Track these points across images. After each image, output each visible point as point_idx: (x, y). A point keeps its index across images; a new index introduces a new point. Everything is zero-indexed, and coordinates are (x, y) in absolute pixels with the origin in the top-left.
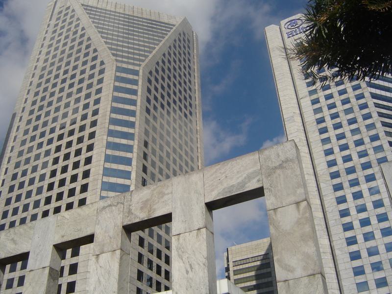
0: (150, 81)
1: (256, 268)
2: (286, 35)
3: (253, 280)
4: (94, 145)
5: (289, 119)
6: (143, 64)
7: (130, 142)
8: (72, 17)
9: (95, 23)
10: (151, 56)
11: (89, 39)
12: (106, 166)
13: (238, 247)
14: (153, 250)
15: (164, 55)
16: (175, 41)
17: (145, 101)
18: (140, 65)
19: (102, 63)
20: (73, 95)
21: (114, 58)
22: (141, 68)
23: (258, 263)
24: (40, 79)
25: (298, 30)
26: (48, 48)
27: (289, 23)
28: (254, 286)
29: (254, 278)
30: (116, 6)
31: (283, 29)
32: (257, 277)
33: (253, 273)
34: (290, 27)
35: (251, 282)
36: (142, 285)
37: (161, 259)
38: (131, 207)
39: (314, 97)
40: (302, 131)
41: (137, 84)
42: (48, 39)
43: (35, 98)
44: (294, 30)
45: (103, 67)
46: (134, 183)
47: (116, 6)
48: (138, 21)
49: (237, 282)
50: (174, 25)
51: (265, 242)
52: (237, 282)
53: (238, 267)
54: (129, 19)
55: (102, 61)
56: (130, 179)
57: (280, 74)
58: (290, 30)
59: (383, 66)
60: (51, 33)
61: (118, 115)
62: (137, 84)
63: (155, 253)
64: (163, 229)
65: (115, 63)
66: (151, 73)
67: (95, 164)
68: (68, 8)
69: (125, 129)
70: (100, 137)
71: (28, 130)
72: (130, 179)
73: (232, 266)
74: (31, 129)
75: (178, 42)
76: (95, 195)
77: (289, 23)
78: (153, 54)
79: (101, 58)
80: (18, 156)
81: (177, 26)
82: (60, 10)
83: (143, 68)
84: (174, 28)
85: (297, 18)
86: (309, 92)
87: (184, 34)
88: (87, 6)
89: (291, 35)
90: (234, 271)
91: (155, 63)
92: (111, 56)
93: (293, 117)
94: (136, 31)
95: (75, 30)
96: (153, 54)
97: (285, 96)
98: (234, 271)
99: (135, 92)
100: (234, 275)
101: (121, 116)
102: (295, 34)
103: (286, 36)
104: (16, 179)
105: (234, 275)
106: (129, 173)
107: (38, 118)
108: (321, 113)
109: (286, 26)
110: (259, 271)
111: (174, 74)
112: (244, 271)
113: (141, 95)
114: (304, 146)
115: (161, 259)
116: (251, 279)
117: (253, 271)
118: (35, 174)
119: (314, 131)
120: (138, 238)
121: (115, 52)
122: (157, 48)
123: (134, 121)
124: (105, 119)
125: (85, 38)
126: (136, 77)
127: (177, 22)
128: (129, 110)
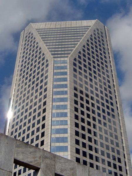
0: (75, 64)
6: (69, 56)
8: (32, 38)
11: (40, 48)
15: (84, 46)
16: (91, 36)
18: (67, 57)
21: (53, 56)
22: (68, 58)
37: (119, 166)
45: (47, 63)
47: (56, 25)
50: (90, 26)
56: (67, 125)
59: (10, 115)
61: (57, 89)
64: (93, 150)
65: (53, 59)
69: (62, 96)
71: (45, 92)
74: (38, 95)
76: (48, 138)
78: (76, 48)
84: (90, 28)
87: (98, 30)
88: (39, 29)
91: (77, 53)
92: (51, 55)
95: (33, 45)
104: (34, 126)
106: (67, 129)
107: (41, 87)
111: (92, 56)
113: (69, 74)
115: (119, 166)
121: (54, 53)
122: (79, 43)
123: (67, 90)
125: (39, 48)
127: (92, 24)
128: (63, 84)
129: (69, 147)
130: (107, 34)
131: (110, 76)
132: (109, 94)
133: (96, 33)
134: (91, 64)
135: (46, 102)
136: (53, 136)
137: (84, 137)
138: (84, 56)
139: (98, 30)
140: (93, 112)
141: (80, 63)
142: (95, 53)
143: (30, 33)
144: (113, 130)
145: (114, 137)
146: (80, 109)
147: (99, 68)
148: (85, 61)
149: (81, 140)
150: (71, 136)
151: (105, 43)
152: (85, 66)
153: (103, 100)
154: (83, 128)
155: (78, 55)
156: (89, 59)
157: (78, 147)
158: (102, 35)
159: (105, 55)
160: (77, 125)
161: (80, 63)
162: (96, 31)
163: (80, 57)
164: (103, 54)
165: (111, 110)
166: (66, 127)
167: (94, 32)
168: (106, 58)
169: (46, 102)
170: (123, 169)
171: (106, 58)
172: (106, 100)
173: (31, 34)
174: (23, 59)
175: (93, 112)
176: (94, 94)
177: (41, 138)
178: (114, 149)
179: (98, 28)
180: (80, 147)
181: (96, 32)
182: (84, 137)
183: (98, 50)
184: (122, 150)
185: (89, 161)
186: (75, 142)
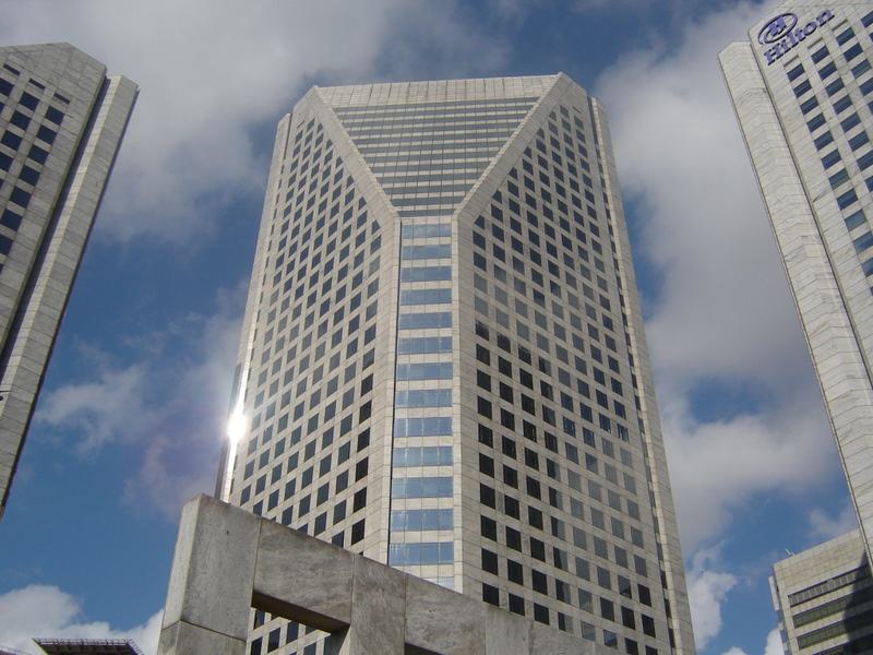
0: (479, 240)
1: (844, 605)
2: (765, 57)
3: (840, 634)
5: (793, 254)
6: (459, 207)
8: (319, 140)
9: (355, 133)
10: (477, 184)
13: (795, 558)
14: (630, 588)
18: (451, 212)
19: (376, 226)
20: (331, 306)
21: (398, 209)
22: (455, 217)
23: (848, 591)
25: (788, 40)
27: (767, 30)
28: (845, 646)
29: (842, 629)
30: (408, 92)
31: (757, 46)
32: (849, 625)
33: (838, 617)
34: (770, 38)
35: (837, 638)
38: (365, 555)
39: (843, 188)
40: (827, 277)
44: (780, 41)
45: (377, 234)
46: (460, 472)
48: (475, 110)
49: (804, 641)
51: (856, 540)
52: (804, 642)
53: (802, 606)
54: (435, 113)
55: (376, 221)
56: (450, 463)
57: (763, 153)
58: (771, 46)
63: (635, 594)
65: (398, 221)
67: (374, 445)
68: (311, 124)
70: (381, 386)
72: (450, 463)
73: (788, 606)
77: (767, 30)
78: (482, 179)
81: (543, 97)
83: (460, 215)
84: (536, 105)
85: (783, 13)
86: (830, 179)
87: (564, 111)
89: (775, 56)
90: (795, 617)
93: (802, 247)
94: (460, 137)
95: (325, 168)
96: (482, 179)
97: (779, 201)
98: (795, 617)
99: (445, 274)
100: (797, 626)
101: (420, 331)
102: (782, 51)
103: (764, 60)
105: (797, 626)
108: (864, 225)
109: (762, 39)
110: (852, 609)
112: (818, 614)
114: (836, 312)
116: (835, 630)
117: (838, 611)
118: (340, 472)
119: (853, 271)
122: (494, 161)
124: (388, 346)
125: (344, 180)
128: (436, 314)
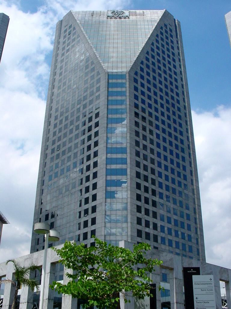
0: (136, 81)
4: (99, 141)
7: (124, 156)
12: (108, 167)
17: (133, 99)
24: (63, 50)
26: (64, 33)
36: (141, 240)
41: (126, 163)
42: (61, 43)
43: (63, 52)
60: (63, 33)
62: (126, 163)
66: (136, 73)
75: (160, 36)
79: (97, 69)
80: (52, 153)
82: (65, 29)
87: (166, 26)
106: (126, 170)
120: (136, 207)
126: (124, 166)
129: (128, 171)
130: (178, 31)
131: (175, 42)
132: (178, 120)
133: (163, 31)
134: (157, 79)
135: (98, 122)
136: (110, 90)
137: (146, 179)
138: (148, 67)
139: (166, 26)
140: (156, 110)
141: (142, 77)
142: (162, 61)
143: (70, 27)
144: (181, 168)
145: (183, 177)
146: (142, 142)
147: (164, 62)
148: (148, 74)
149: (143, 184)
150: (131, 179)
151: (175, 45)
152: (149, 82)
153: (171, 129)
154: (145, 168)
155: (139, 67)
156: (154, 71)
157: (139, 192)
158: (172, 34)
159: (174, 63)
160: (138, 164)
161: (142, 77)
162: (164, 28)
163: (142, 70)
164: (172, 62)
165: (180, 142)
166: (124, 156)
167: (161, 30)
168: (176, 69)
169: (98, 122)
170: (192, 218)
171: (176, 69)
172: (171, 97)
173: (72, 29)
174: (64, 46)
175: (156, 110)
176: (159, 121)
177: (94, 147)
178: (181, 183)
179: (167, 23)
180: (140, 149)
181: (164, 30)
182: (146, 179)
183: (166, 57)
184: (193, 214)
185: (146, 92)
186: (135, 186)
